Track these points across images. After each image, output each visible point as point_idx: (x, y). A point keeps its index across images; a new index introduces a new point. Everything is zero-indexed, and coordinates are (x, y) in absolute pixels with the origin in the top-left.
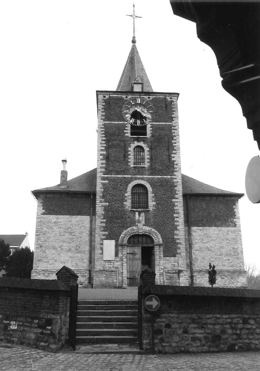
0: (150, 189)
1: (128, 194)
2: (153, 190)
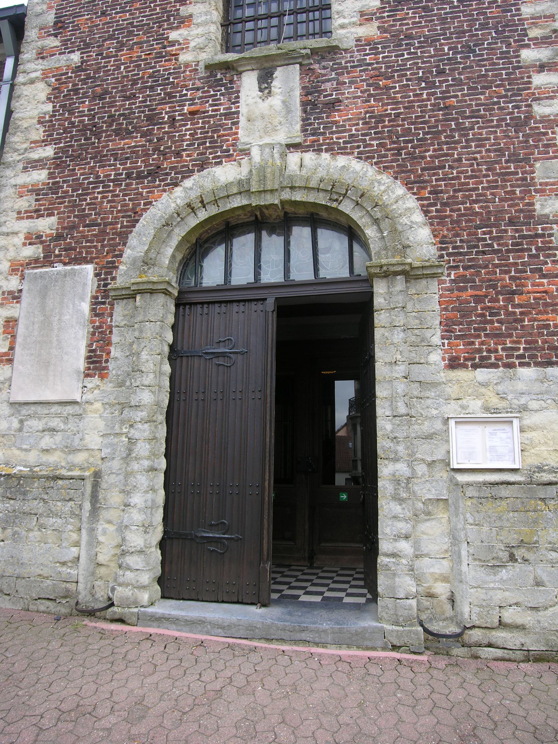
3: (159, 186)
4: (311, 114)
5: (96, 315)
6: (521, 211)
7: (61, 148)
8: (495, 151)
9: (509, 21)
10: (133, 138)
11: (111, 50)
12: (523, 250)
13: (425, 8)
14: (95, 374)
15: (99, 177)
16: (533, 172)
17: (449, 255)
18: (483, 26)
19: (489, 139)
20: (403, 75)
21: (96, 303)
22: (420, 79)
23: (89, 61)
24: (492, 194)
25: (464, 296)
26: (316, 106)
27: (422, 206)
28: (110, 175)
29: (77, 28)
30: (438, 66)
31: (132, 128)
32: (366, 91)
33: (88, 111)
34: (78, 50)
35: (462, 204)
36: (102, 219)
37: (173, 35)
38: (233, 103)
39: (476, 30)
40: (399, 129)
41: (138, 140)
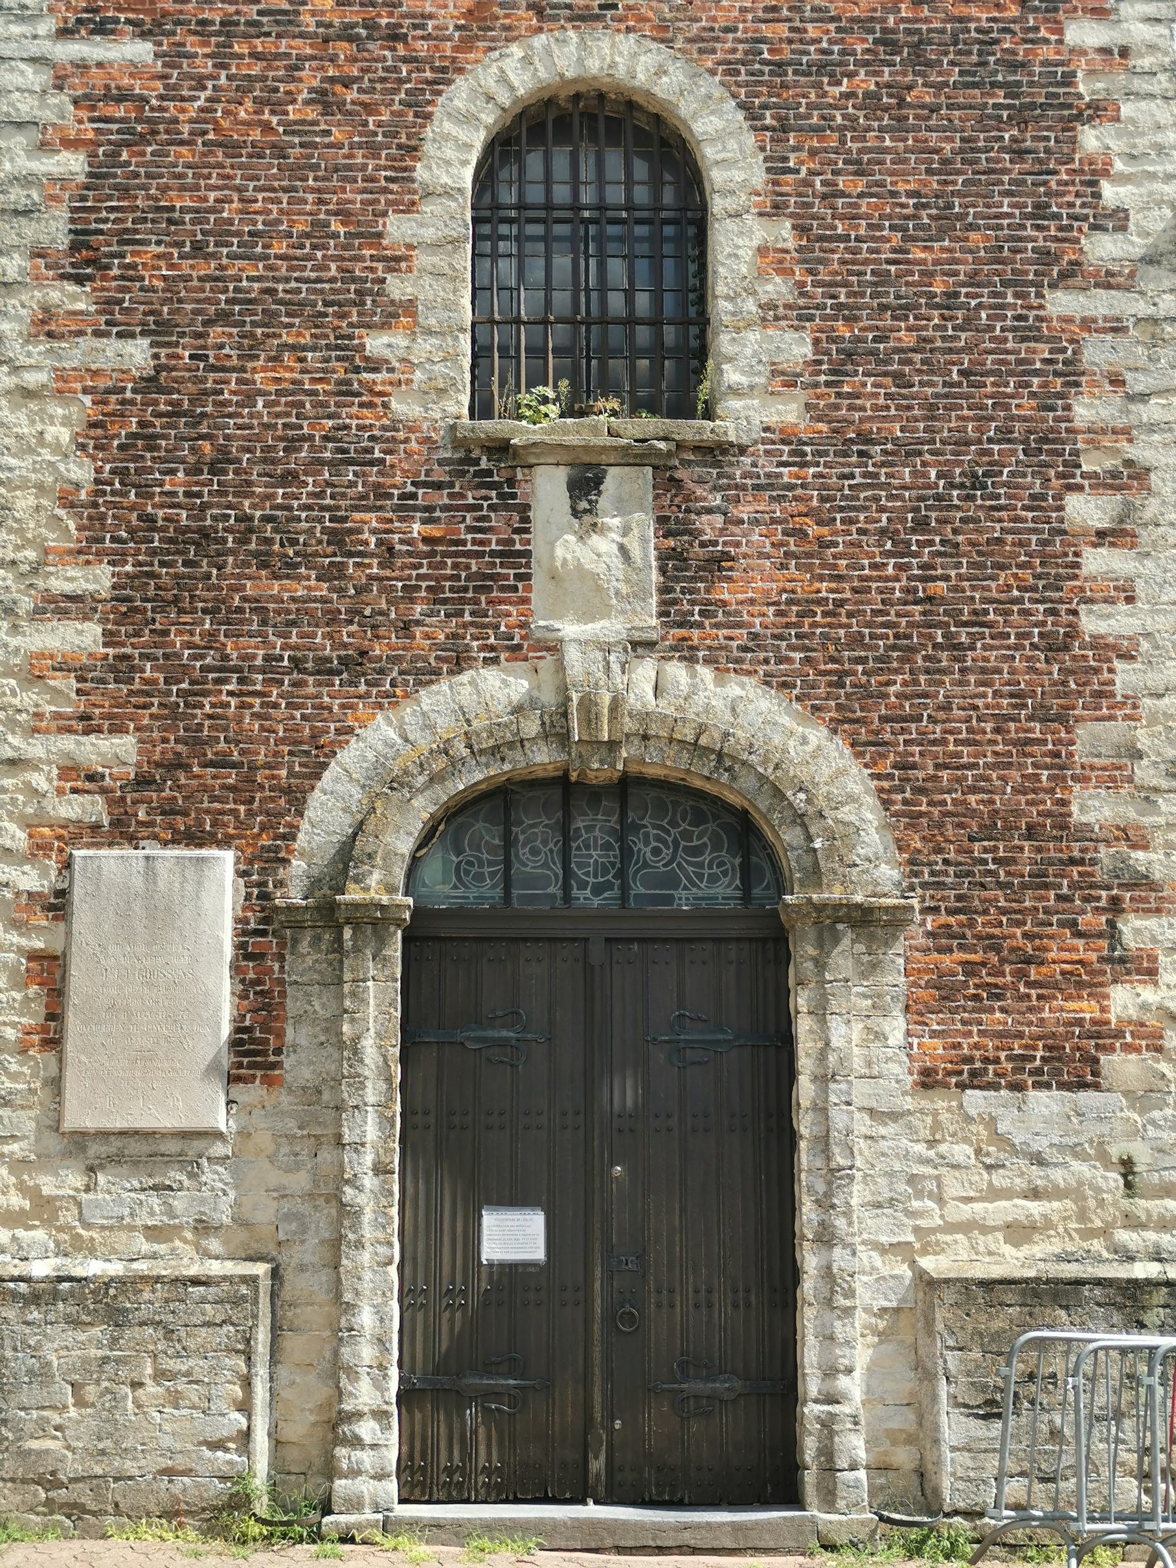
1: (452, 155)
3: (368, 695)
4: (677, 579)
5: (248, 957)
7: (127, 574)
8: (1012, 695)
9: (1052, 430)
10: (299, 578)
12: (1046, 886)
15: (225, 658)
16: (1072, 743)
17: (924, 885)
18: (1005, 434)
20: (851, 521)
21: (244, 933)
22: (883, 532)
23: (174, 369)
24: (1000, 778)
26: (688, 568)
27: (881, 790)
28: (254, 657)
29: (130, 275)
32: (782, 544)
33: (188, 494)
35: (949, 792)
37: (376, 344)
38: (517, 531)
39: (990, 440)
40: (842, 632)
41: (308, 586)
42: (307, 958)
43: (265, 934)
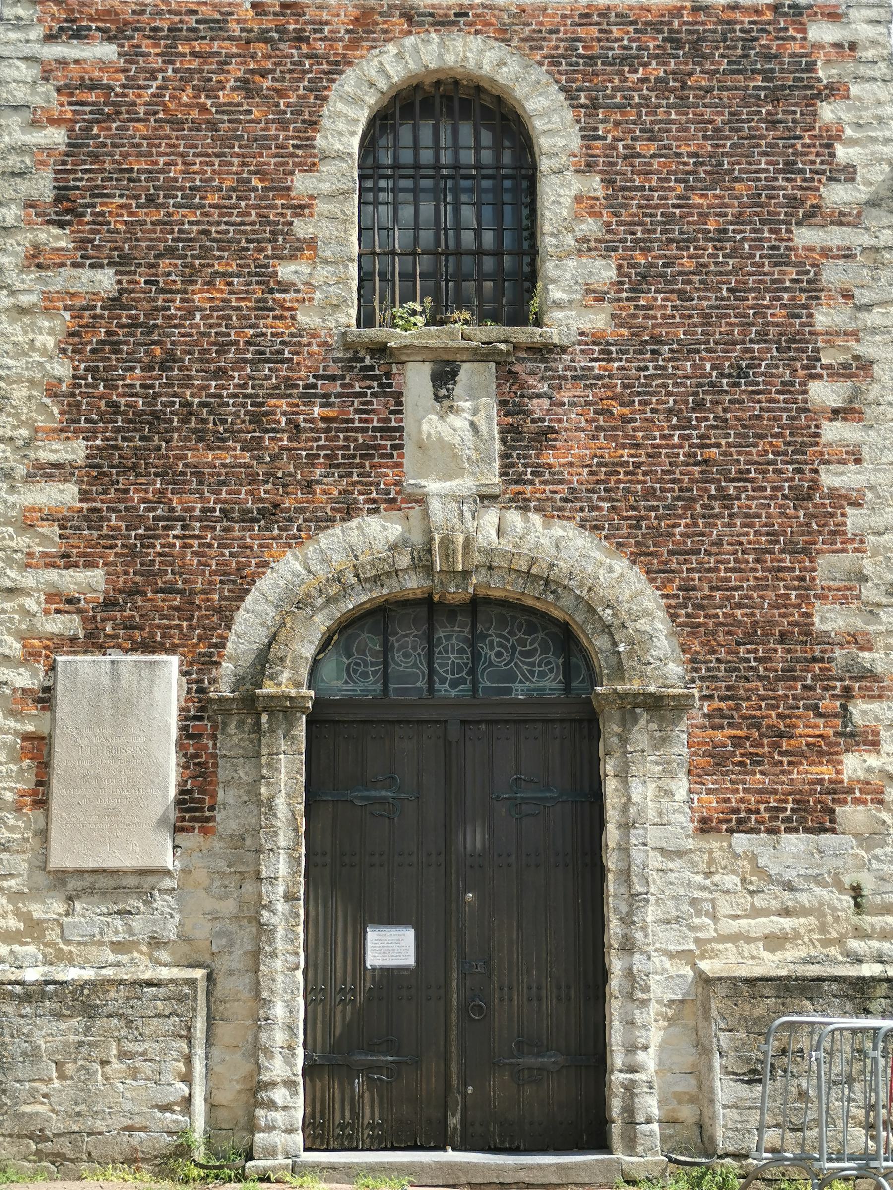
0: (554, 127)
1: (343, 128)
2: (589, 136)
3: (280, 537)
4: (514, 448)
5: (189, 737)
6: (796, 624)
7: (98, 447)
9: (798, 333)
10: (227, 449)
11: (173, 277)
12: (795, 679)
13: (681, 293)
14: (194, 828)
15: (172, 510)
17: (702, 679)
19: (758, 516)
21: (186, 719)
22: (670, 411)
23: (133, 291)
24: (759, 597)
25: (719, 736)
26: (522, 439)
27: (669, 607)
29: (99, 220)
30: (695, 394)
31: (226, 431)
32: (594, 421)
33: (143, 386)
34: (109, 264)
36: (185, 581)
37: (286, 271)
38: (393, 412)
39: (751, 341)
40: (639, 487)
41: (235, 455)
42: (233, 738)
43: (202, 719)
